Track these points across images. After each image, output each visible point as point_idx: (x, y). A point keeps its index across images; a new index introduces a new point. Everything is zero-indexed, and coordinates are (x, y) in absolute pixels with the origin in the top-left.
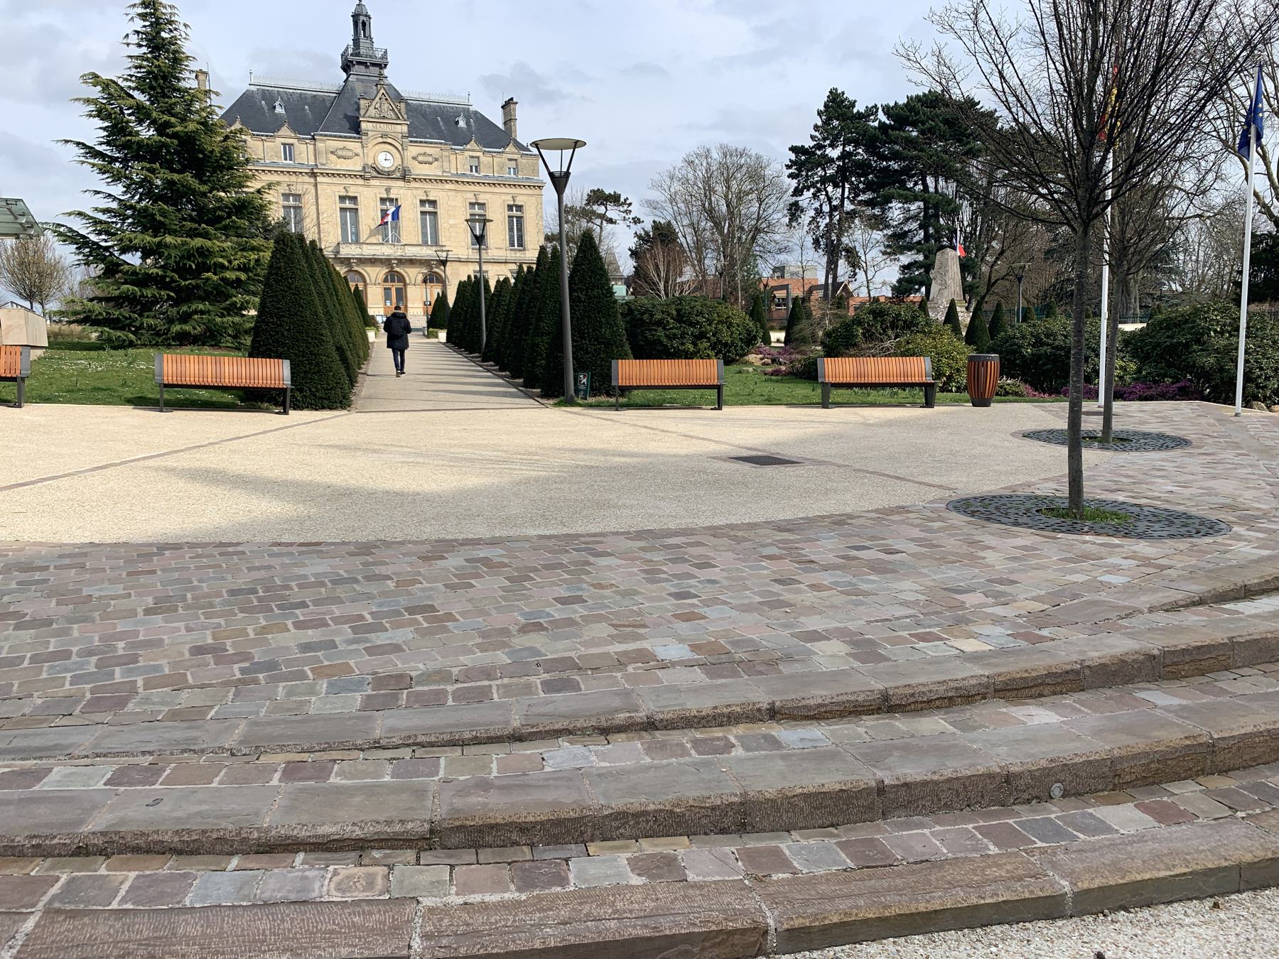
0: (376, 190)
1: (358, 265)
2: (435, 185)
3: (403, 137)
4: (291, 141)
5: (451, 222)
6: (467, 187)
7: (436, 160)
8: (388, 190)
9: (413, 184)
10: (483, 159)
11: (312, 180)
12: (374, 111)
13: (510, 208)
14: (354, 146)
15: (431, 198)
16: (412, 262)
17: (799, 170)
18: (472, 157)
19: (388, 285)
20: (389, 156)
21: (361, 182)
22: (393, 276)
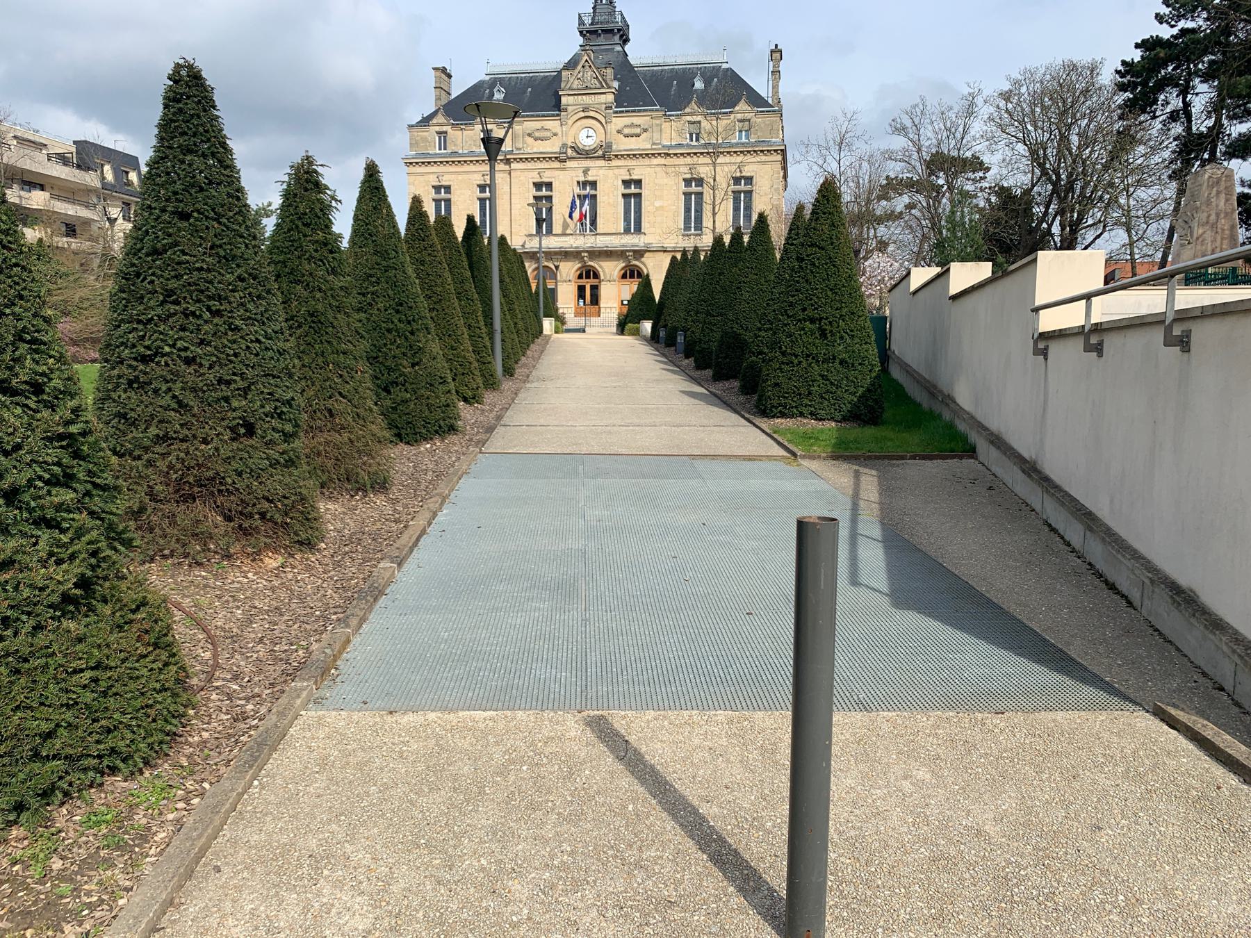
0: (573, 173)
1: (591, 258)
2: (641, 161)
3: (606, 108)
4: (444, 129)
5: (657, 204)
6: (681, 161)
7: (645, 130)
8: (586, 171)
9: (615, 163)
10: (705, 124)
11: (507, 168)
12: (576, 82)
13: (688, 182)
14: (553, 125)
15: (635, 177)
16: (608, 254)
17: (1127, 72)
18: (694, 123)
19: (583, 282)
20: (591, 132)
21: (556, 164)
22: (589, 273)
